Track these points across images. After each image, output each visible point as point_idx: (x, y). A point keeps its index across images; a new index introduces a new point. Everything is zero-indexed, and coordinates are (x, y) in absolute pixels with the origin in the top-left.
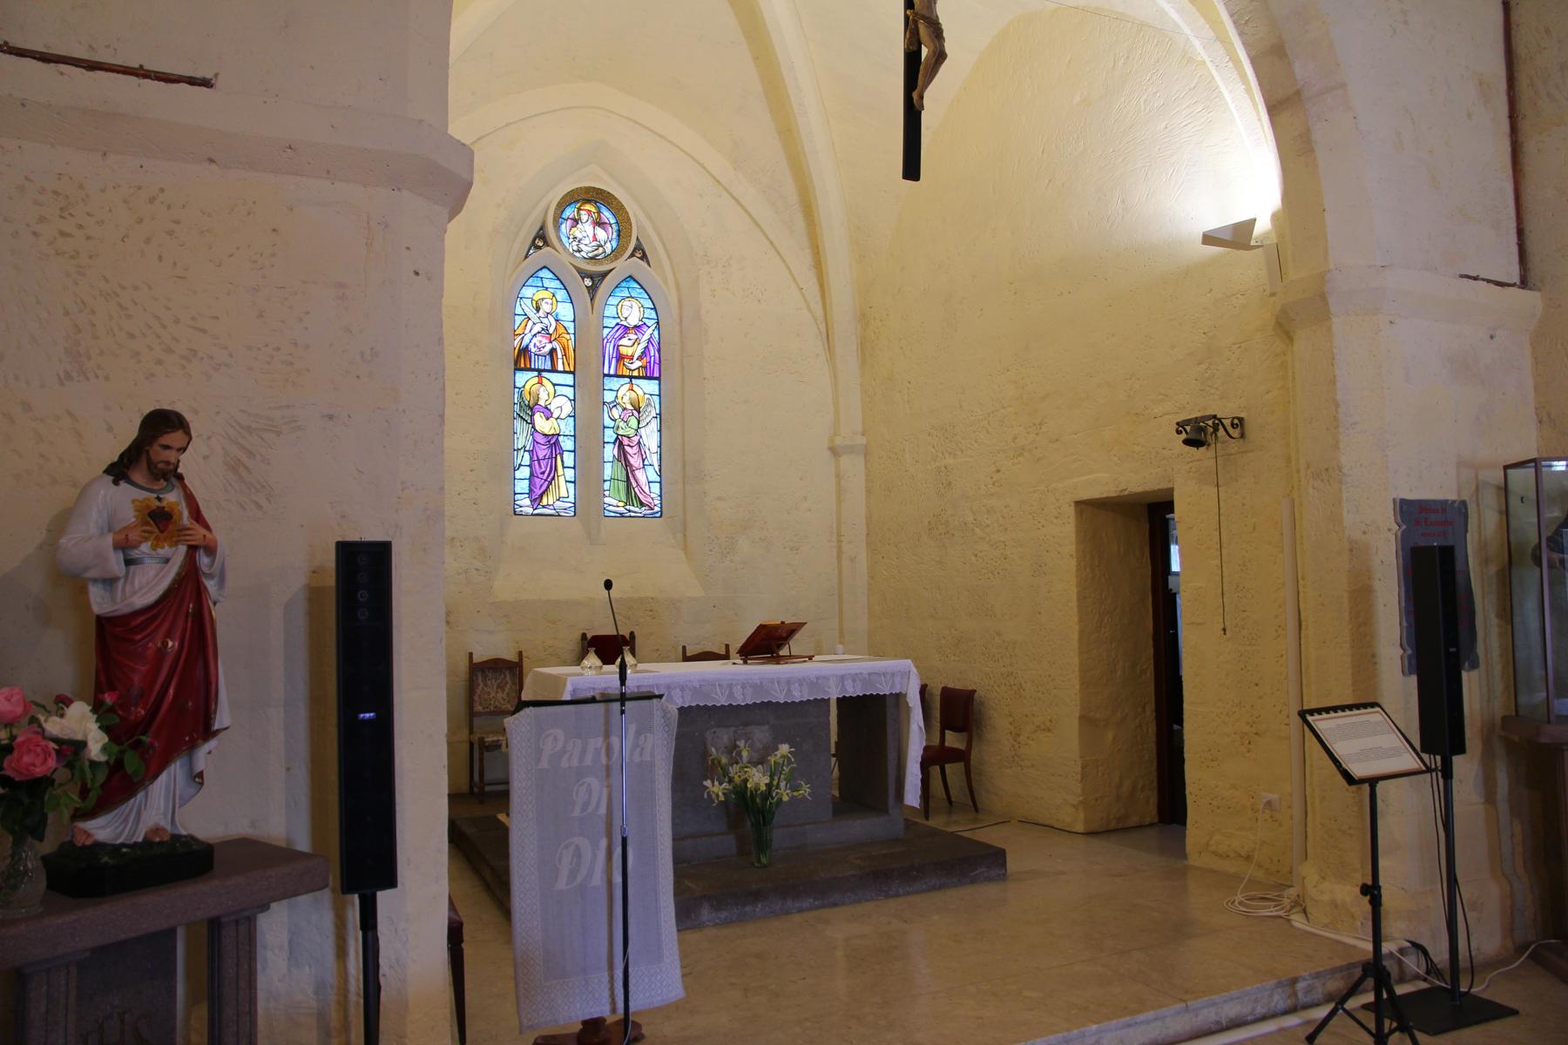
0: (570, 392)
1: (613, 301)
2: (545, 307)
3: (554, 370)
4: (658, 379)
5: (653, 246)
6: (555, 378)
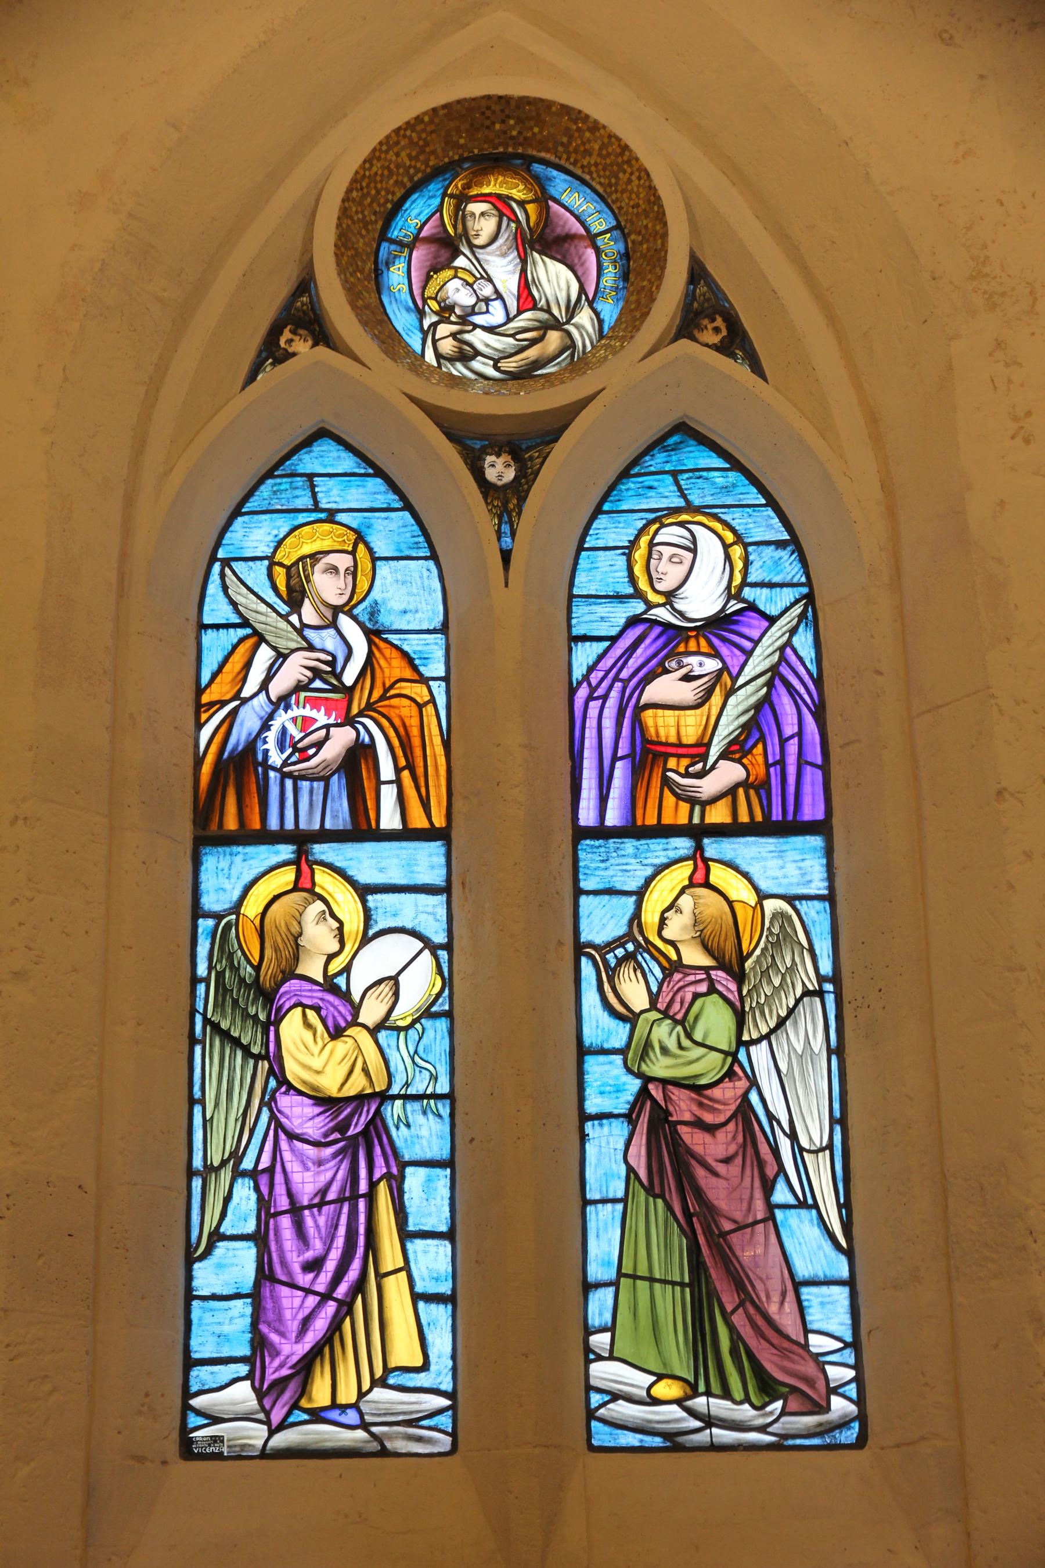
0: (429, 914)
1: (611, 531)
2: (329, 587)
3: (363, 830)
4: (820, 828)
5: (765, 282)
6: (367, 861)
